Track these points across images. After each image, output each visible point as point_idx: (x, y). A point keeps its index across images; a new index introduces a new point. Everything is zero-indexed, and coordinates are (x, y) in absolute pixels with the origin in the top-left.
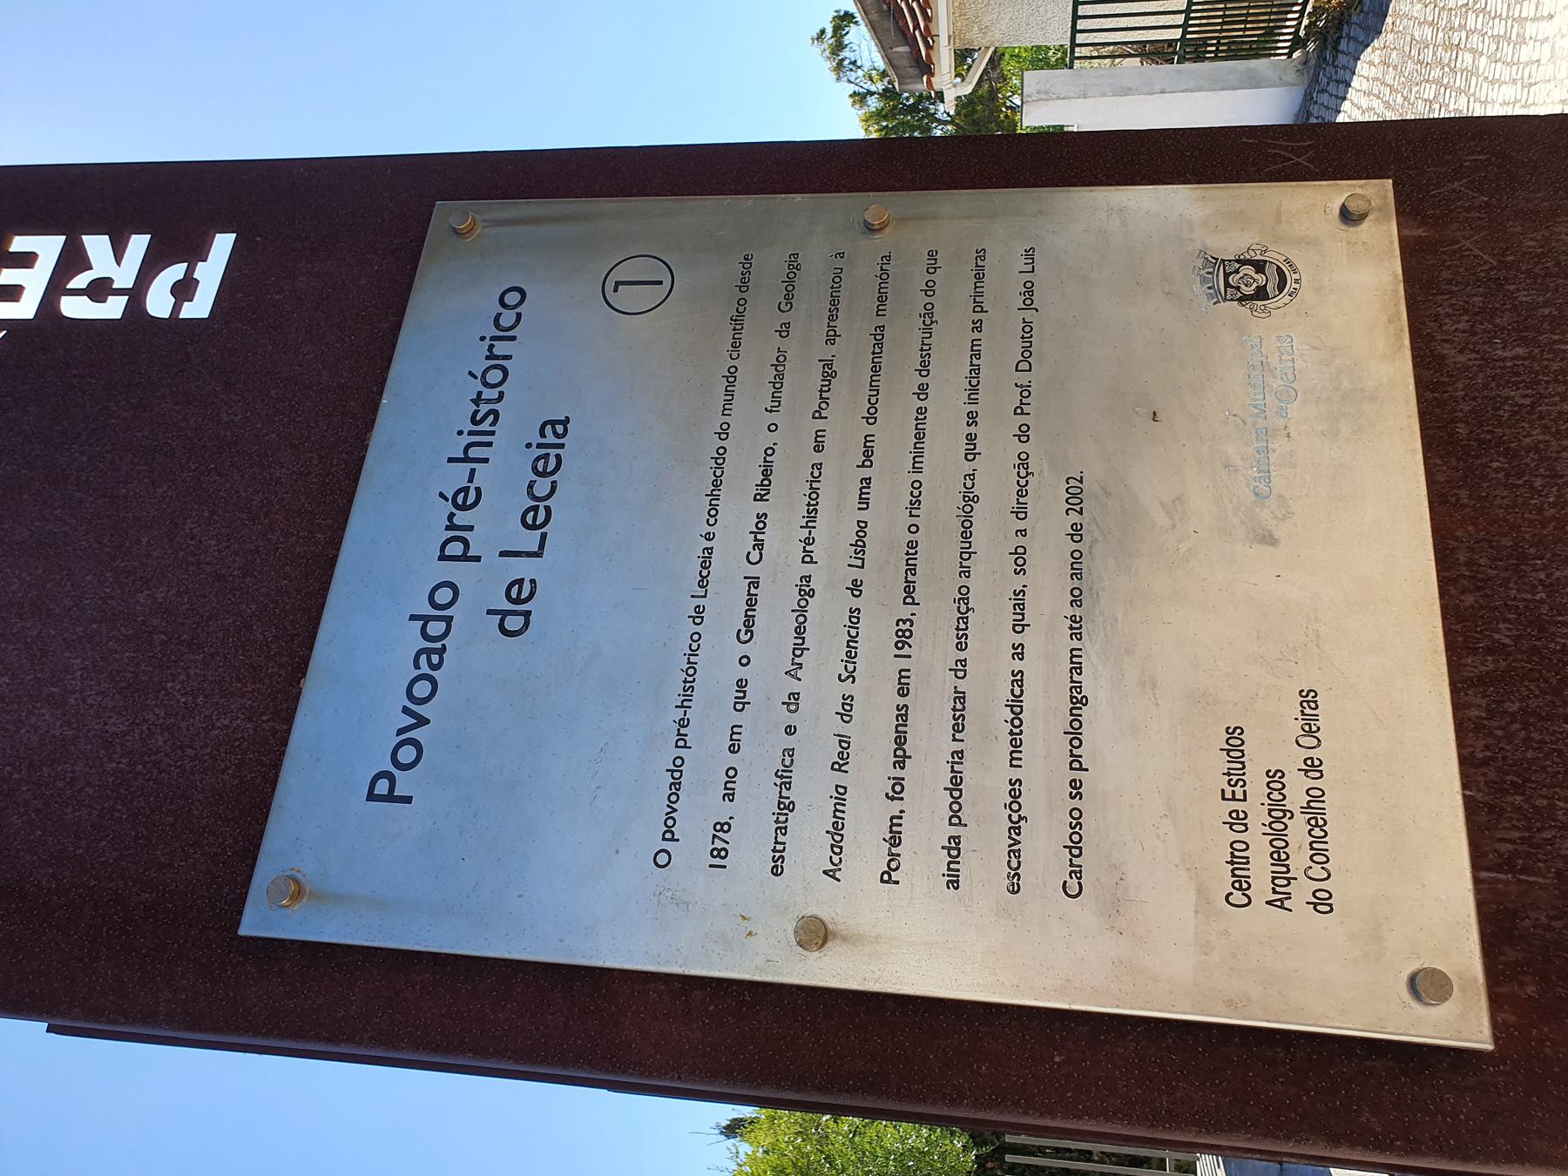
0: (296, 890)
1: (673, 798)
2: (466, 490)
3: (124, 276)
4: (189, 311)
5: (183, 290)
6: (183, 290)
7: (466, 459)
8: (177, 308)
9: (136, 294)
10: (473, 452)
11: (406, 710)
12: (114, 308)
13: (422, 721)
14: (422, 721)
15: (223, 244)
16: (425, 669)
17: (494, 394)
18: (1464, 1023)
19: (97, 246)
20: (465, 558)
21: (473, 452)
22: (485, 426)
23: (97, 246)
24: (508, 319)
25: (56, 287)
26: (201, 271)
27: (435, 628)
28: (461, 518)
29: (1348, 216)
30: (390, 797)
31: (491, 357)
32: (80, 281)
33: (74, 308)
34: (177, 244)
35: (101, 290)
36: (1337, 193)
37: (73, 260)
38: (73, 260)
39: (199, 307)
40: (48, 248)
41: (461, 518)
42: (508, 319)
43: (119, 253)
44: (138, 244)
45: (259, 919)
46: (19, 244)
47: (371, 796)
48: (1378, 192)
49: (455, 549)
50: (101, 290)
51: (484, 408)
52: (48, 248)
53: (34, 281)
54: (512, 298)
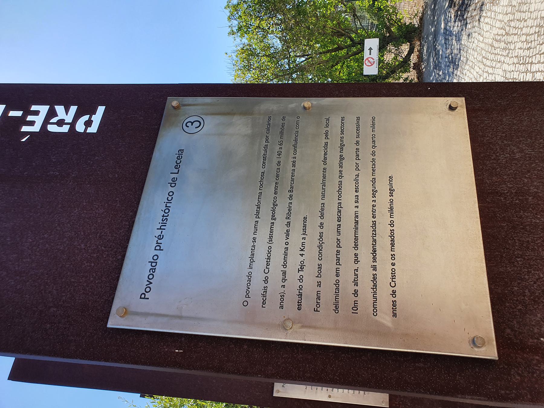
0: (126, 312)
1: (249, 284)
2: (160, 235)
3: (69, 118)
4: (90, 130)
5: (88, 124)
6: (88, 124)
7: (161, 229)
8: (86, 129)
9: (73, 125)
10: (162, 227)
11: (148, 281)
12: (65, 129)
13: (151, 283)
14: (151, 283)
15: (101, 110)
16: (151, 273)
17: (167, 215)
18: (490, 352)
19: (60, 109)
20: (160, 250)
21: (162, 227)
22: (165, 222)
23: (60, 109)
24: (170, 198)
25: (46, 122)
26: (94, 118)
27: (154, 264)
28: (159, 241)
29: (451, 108)
30: (144, 298)
31: (166, 207)
32: (54, 120)
33: (52, 128)
34: (86, 109)
35: (61, 123)
36: (450, 100)
37: (52, 113)
38: (52, 113)
39: (93, 129)
40: (44, 109)
41: (159, 241)
42: (170, 198)
43: (67, 112)
44: (73, 109)
45: (114, 322)
46: (34, 108)
47: (141, 298)
48: (460, 102)
49: (158, 248)
50: (61, 123)
51: (165, 218)
52: (44, 109)
53: (39, 120)
54: (171, 194)
